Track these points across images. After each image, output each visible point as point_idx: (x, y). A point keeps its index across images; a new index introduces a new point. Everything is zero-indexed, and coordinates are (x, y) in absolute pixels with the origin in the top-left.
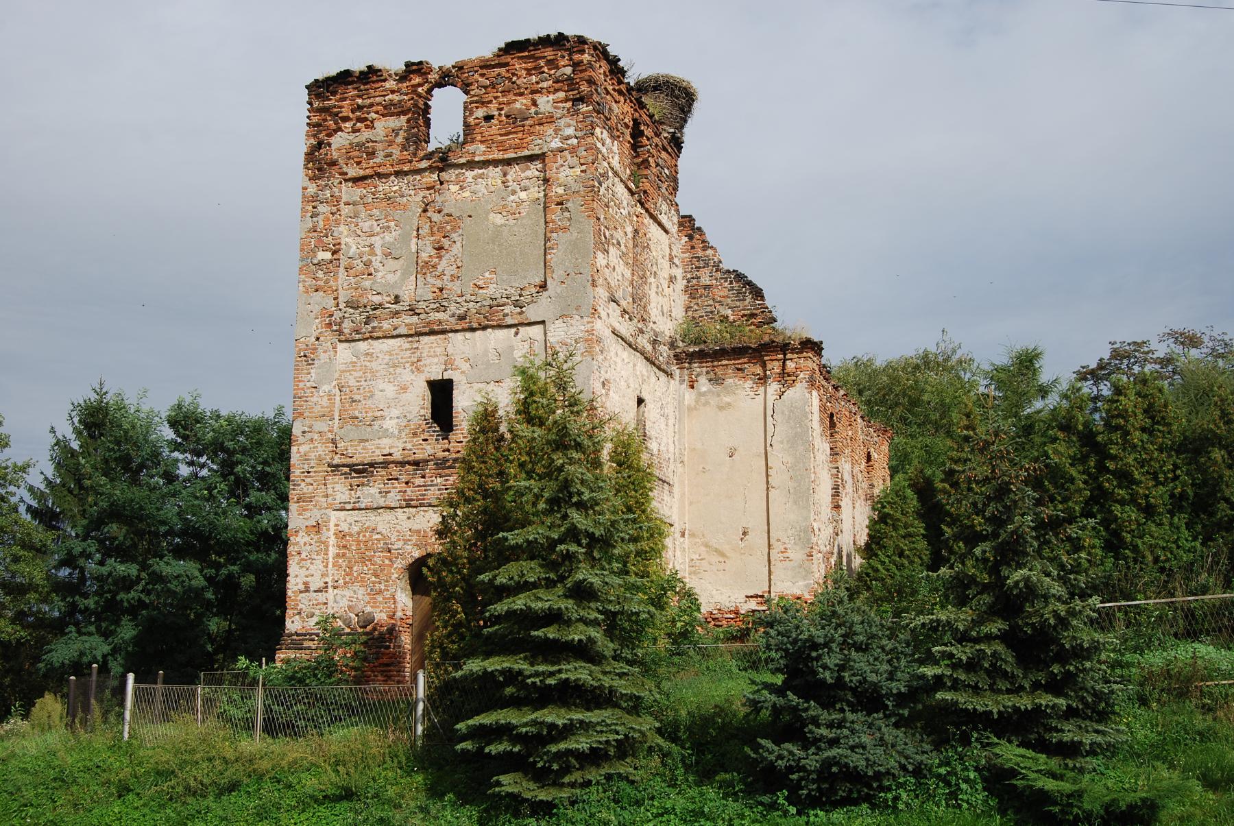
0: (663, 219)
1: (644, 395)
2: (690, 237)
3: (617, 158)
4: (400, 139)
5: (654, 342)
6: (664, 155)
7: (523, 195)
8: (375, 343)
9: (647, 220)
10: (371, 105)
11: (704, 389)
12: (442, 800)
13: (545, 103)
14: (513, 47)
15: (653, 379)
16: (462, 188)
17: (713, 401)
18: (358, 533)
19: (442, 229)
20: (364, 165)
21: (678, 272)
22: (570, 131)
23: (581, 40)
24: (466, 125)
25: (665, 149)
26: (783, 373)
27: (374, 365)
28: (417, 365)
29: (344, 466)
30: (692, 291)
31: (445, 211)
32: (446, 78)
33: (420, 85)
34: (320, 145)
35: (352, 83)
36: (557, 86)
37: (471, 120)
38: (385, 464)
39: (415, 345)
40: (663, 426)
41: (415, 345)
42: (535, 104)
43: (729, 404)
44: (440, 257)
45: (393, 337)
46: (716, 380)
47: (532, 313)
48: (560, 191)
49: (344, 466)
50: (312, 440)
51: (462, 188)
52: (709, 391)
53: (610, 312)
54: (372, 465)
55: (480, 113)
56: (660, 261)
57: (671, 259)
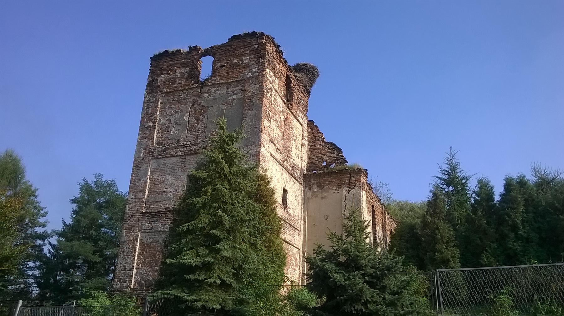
0: (301, 120)
1: (287, 188)
2: (312, 129)
3: (277, 85)
4: (185, 77)
5: (293, 167)
6: (301, 94)
7: (234, 97)
8: (167, 159)
9: (292, 117)
10: (176, 64)
11: (315, 190)
12: (122, 287)
13: (246, 60)
14: (235, 38)
15: (292, 183)
16: (209, 95)
17: (320, 195)
18: (150, 243)
19: (199, 113)
20: (170, 87)
21: (306, 143)
22: (255, 70)
23: (262, 34)
24: (213, 70)
25: (302, 93)
26: (350, 183)
27: (165, 169)
28: (184, 170)
29: (147, 213)
30: (311, 150)
32: (207, 53)
33: (195, 55)
34: (153, 80)
35: (169, 55)
36: (251, 53)
37: (215, 68)
38: (165, 212)
39: (184, 160)
40: (296, 204)
41: (184, 160)
42: (242, 60)
43: (326, 196)
44: (198, 124)
45: (175, 156)
46: (320, 186)
48: (250, 94)
49: (147, 213)
50: (135, 202)
51: (209, 95)
52: (318, 191)
53: (270, 146)
54: (159, 212)
55: (219, 65)
56: (298, 136)
57: (303, 136)
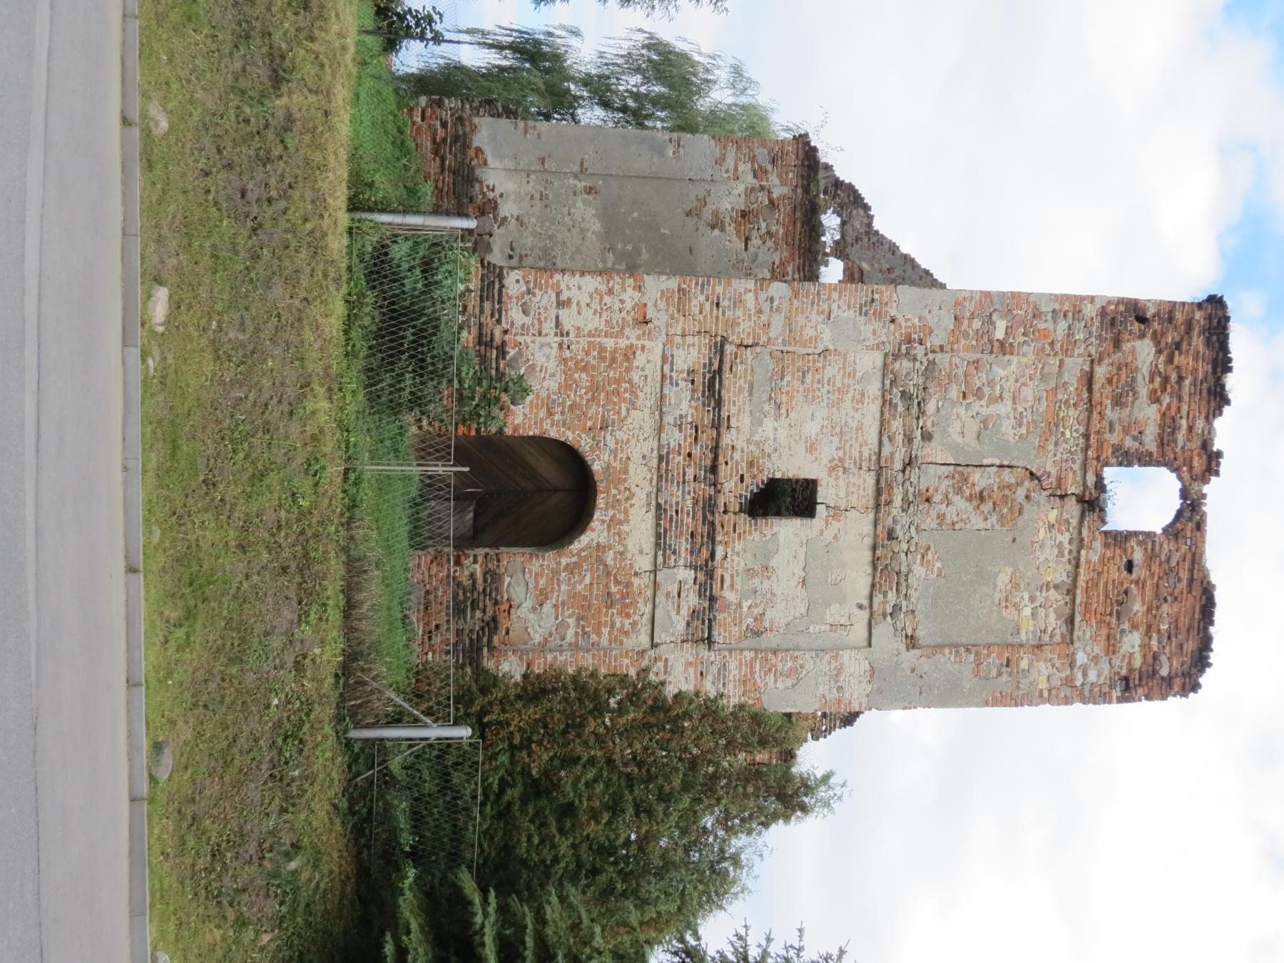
31: (1026, 506)
35: (1214, 372)
47: (883, 630)
